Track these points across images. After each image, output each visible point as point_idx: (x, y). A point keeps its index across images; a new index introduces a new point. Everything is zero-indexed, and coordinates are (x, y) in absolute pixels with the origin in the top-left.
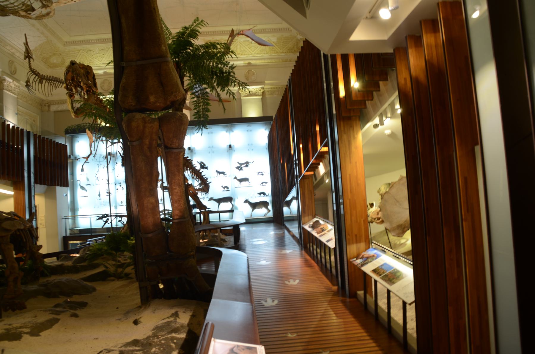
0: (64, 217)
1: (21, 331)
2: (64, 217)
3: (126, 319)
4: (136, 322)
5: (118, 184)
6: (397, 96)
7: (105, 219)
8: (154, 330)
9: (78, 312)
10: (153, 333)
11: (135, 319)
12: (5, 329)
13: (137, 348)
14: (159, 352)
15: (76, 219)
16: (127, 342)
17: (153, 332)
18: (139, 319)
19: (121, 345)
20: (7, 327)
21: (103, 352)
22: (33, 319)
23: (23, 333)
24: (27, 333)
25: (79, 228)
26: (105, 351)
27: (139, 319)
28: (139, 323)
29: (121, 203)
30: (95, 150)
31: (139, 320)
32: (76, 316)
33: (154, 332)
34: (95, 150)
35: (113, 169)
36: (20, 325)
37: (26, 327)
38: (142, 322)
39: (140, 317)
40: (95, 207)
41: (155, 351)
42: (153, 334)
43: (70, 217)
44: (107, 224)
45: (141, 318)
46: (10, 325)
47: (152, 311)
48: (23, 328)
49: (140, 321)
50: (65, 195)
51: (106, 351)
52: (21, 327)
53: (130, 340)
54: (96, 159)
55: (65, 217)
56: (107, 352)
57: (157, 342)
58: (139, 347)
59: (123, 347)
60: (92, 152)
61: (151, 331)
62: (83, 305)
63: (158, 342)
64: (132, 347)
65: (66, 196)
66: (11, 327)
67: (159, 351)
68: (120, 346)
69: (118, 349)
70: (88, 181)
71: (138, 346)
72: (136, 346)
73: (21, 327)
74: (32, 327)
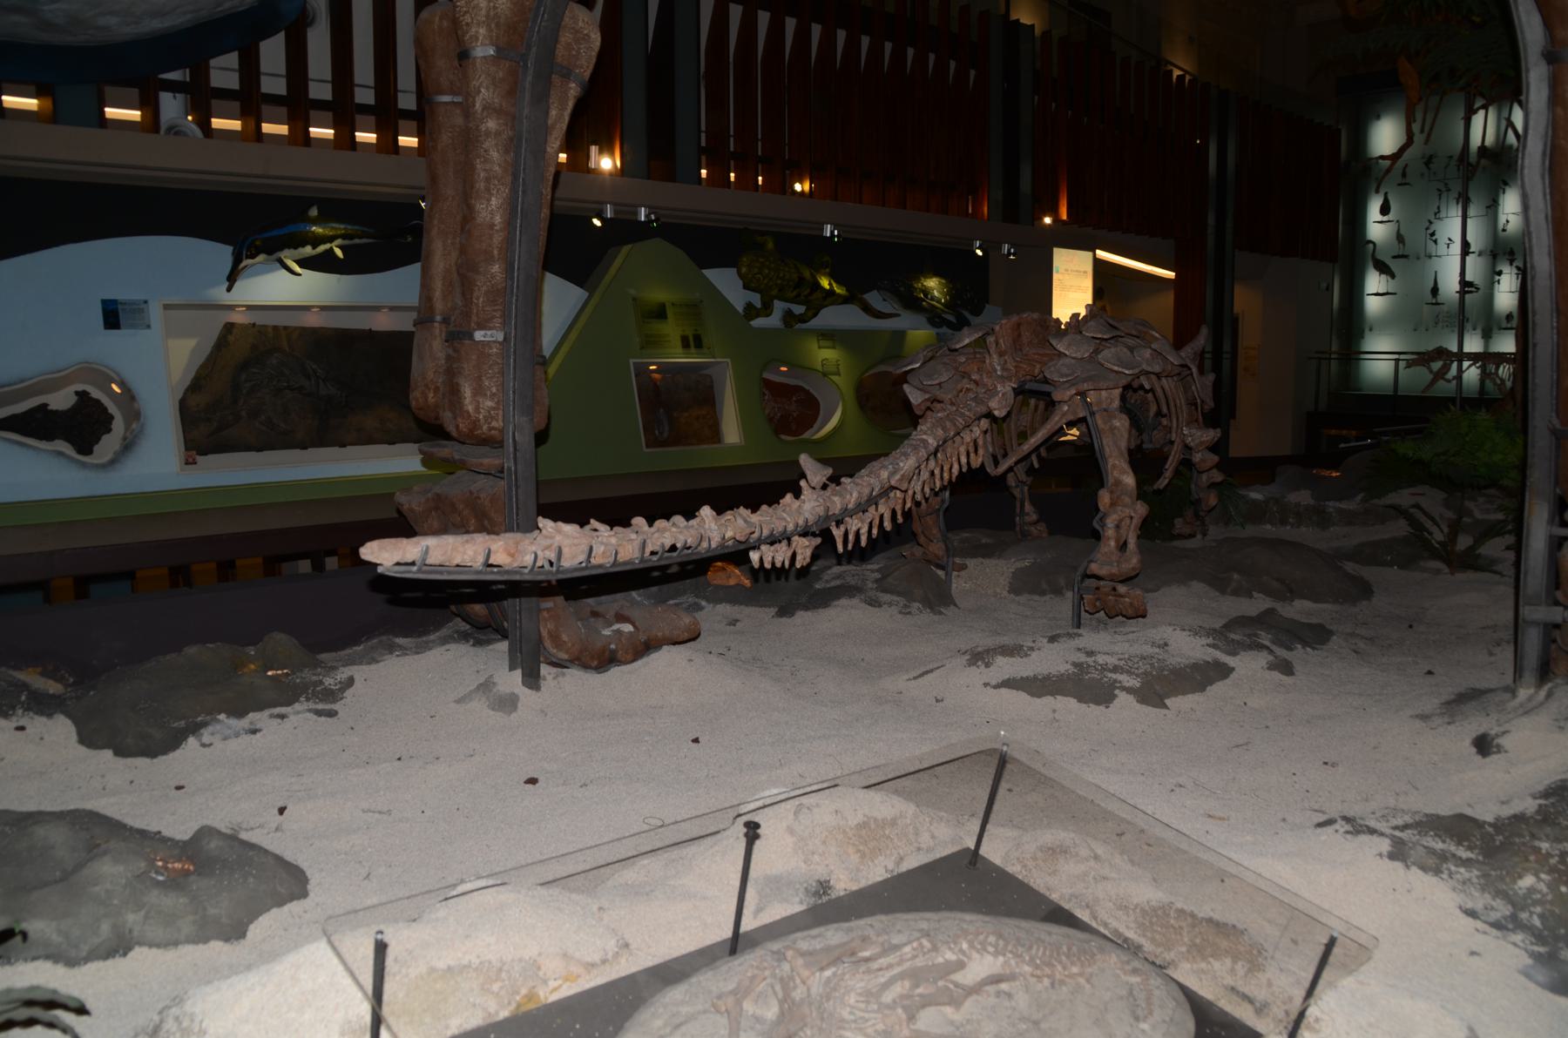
0: (1317, 352)
1: (1115, 681)
2: (1317, 352)
3: (1449, 723)
4: (1484, 745)
5: (1504, 254)
6: (296, 861)
7: (1436, 365)
8: (1546, 794)
9: (1298, 655)
10: (1540, 806)
11: (1482, 730)
12: (1075, 665)
13: (1464, 854)
14: (1550, 897)
15: (1362, 361)
16: (1430, 810)
17: (1542, 802)
18: (1497, 736)
19: (1408, 819)
20: (1082, 658)
21: (1337, 826)
22: (1157, 650)
23: (1118, 688)
24: (1129, 690)
25: (1360, 390)
26: (1343, 823)
27: (1497, 736)
28: (1495, 750)
29: (1505, 321)
30: (1427, 129)
31: (1500, 741)
32: (1286, 668)
33: (1545, 805)
34: (1427, 129)
35: (1491, 203)
36: (1117, 663)
37: (1129, 673)
38: (1506, 752)
39: (1502, 729)
40: (1415, 330)
41: (1531, 890)
42: (1538, 812)
43: (1333, 356)
44: (1441, 383)
45: (1504, 733)
46: (1090, 653)
47: (1556, 720)
48: (1121, 673)
49: (1498, 746)
50: (1324, 285)
51: (1348, 827)
52: (1116, 669)
53: (1445, 810)
54: (1435, 173)
55: (1319, 355)
56: (1347, 832)
57: (1549, 855)
58: (1470, 848)
59: (1409, 831)
60: (1415, 139)
61: (1535, 797)
62: (1316, 636)
63: (1552, 856)
64: (1444, 842)
65: (1327, 289)
66: (1090, 660)
67: (1547, 894)
68: (1399, 822)
69: (1388, 831)
70: (1401, 245)
71: (1466, 844)
72: (1459, 843)
73: (1116, 669)
74: (1145, 673)
